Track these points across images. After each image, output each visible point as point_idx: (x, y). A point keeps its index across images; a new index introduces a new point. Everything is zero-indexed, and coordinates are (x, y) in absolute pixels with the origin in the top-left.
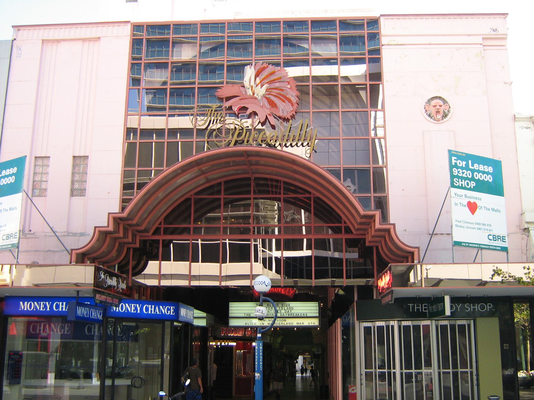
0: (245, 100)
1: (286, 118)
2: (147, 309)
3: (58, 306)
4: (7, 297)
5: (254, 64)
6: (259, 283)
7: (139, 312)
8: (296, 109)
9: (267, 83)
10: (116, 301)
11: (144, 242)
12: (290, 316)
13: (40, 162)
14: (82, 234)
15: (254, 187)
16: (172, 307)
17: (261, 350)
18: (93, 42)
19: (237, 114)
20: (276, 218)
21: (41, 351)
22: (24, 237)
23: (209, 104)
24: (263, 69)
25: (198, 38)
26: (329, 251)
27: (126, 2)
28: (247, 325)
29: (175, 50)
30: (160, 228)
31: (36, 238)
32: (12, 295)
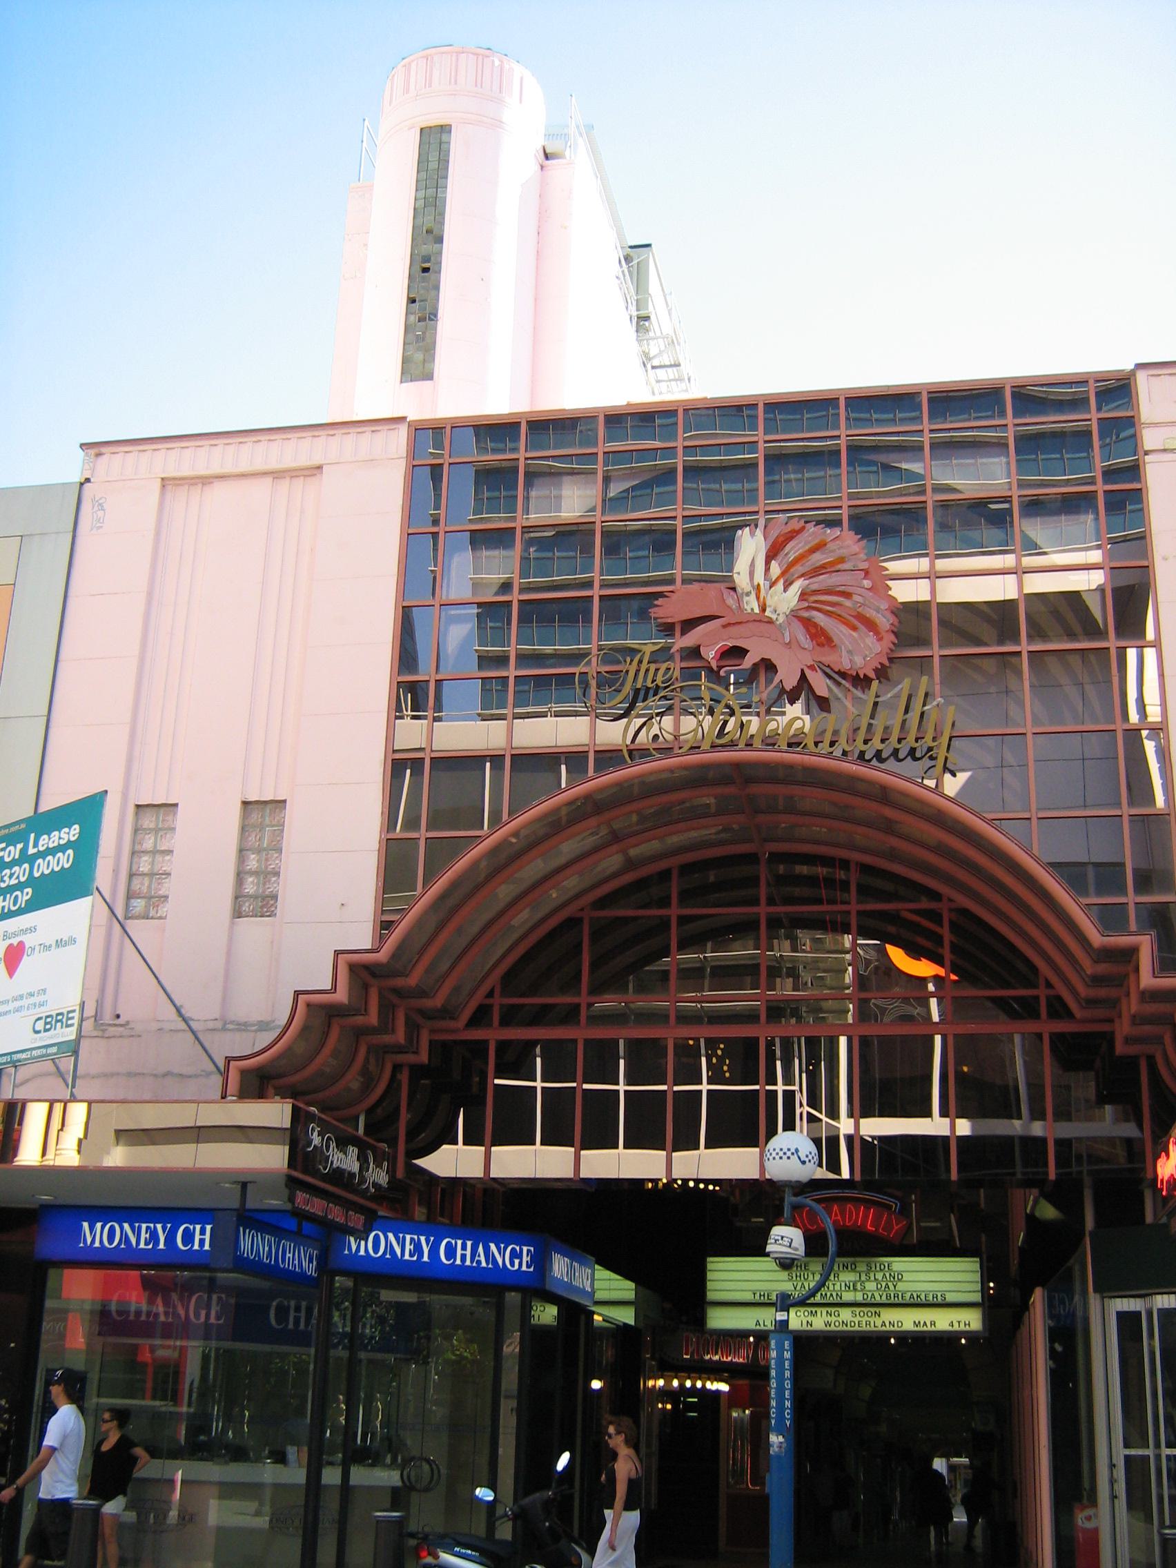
0: (740, 626)
1: (862, 677)
2: (451, 1252)
3: (188, 1237)
4: (46, 1208)
5: (762, 523)
6: (781, 1154)
7: (426, 1258)
8: (891, 650)
9: (802, 575)
10: (357, 1220)
11: (442, 1049)
12: (892, 1301)
13: (148, 821)
14: (263, 1026)
15: (769, 884)
16: (525, 1249)
17: (787, 1363)
18: (302, 478)
19: (715, 668)
20: (849, 1011)
21: (154, 1398)
22: (100, 1034)
23: (630, 642)
24: (792, 535)
25: (600, 457)
26: (1018, 1119)
27: (401, 382)
28: (762, 1327)
29: (533, 493)
30: (490, 1007)
31: (133, 1036)
32: (61, 1202)
